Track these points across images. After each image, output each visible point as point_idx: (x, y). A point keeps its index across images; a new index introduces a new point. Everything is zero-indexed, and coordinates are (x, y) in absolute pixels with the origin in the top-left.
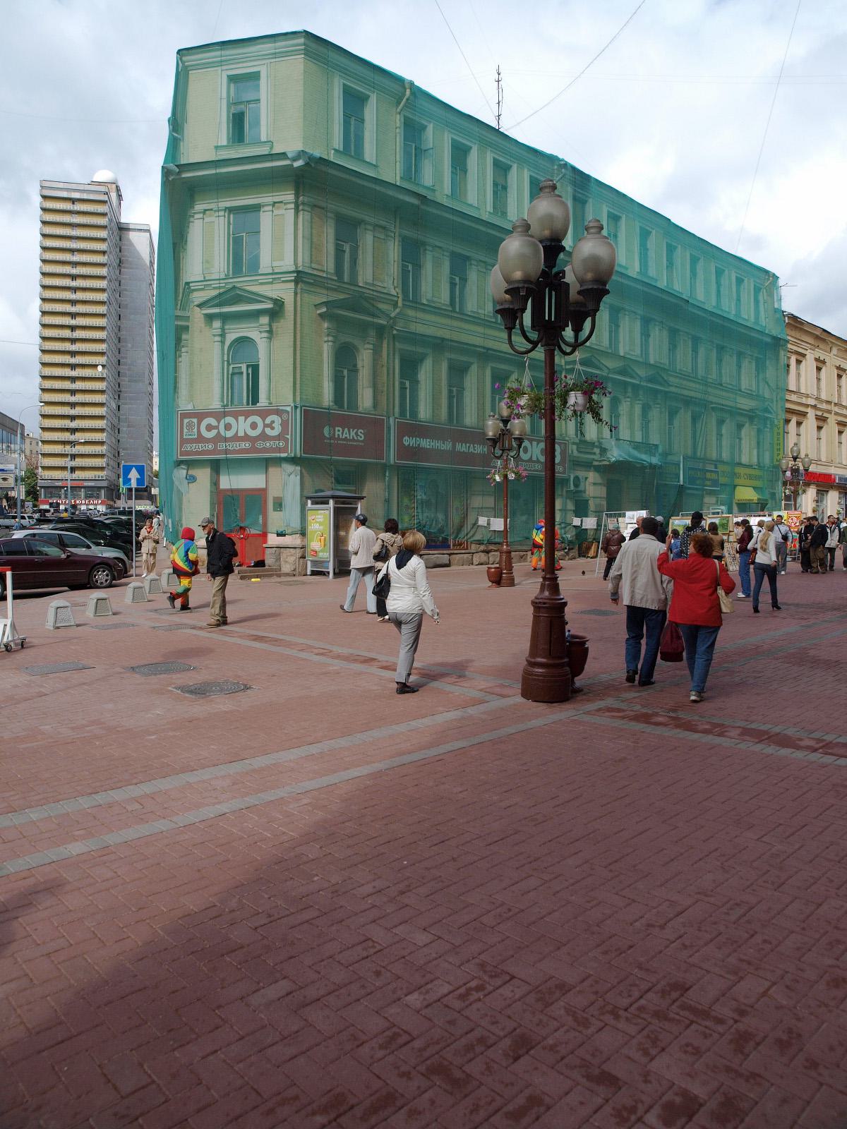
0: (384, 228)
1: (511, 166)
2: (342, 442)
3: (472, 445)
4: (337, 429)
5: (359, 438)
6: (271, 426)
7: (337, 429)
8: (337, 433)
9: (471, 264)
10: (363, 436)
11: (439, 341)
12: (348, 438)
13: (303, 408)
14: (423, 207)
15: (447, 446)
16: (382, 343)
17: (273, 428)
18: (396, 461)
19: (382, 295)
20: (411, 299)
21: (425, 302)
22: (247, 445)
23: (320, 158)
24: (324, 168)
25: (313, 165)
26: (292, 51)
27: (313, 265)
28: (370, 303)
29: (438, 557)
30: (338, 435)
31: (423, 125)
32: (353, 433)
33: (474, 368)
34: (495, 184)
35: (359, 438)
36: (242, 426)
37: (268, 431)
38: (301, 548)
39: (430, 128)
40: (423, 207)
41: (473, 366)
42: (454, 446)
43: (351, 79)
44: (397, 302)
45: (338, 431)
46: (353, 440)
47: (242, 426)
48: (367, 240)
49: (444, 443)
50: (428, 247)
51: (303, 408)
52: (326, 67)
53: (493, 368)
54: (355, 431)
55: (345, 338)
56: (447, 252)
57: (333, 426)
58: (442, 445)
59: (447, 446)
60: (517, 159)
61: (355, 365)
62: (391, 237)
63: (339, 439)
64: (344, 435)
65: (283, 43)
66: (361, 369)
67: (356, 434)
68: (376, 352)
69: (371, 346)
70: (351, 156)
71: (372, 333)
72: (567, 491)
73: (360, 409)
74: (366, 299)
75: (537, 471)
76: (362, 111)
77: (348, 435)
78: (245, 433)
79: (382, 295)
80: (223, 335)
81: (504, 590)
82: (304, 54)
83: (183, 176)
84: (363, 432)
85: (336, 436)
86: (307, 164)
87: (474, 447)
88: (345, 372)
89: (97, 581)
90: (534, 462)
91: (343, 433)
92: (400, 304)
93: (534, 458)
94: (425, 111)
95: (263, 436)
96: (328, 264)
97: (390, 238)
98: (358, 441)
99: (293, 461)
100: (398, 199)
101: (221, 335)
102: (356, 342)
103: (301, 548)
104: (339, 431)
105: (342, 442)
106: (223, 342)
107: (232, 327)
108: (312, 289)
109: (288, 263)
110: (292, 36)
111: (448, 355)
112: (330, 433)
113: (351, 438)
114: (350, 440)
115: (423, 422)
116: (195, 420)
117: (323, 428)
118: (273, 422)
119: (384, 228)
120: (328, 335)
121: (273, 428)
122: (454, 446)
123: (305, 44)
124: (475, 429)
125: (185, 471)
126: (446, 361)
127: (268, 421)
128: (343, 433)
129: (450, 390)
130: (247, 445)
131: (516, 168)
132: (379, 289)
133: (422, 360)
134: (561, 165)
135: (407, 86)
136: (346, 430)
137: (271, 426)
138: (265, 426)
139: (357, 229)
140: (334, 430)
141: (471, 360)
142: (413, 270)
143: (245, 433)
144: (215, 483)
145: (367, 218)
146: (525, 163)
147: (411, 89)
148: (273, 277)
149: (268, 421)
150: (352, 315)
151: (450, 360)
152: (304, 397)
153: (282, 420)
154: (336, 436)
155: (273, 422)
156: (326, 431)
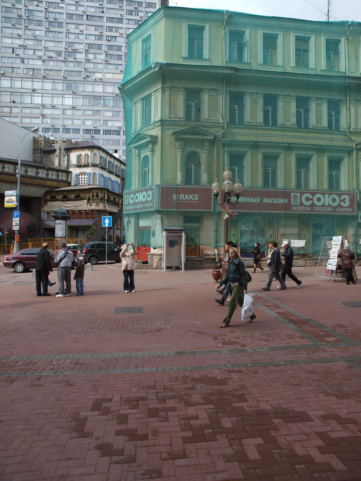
0: (216, 90)
1: (340, 40)
2: (184, 202)
3: (275, 199)
4: (181, 195)
5: (195, 199)
6: (343, 201)
7: (181, 195)
8: (181, 197)
9: (279, 98)
10: (197, 198)
11: (253, 144)
12: (188, 199)
13: (160, 186)
14: (236, 74)
15: (257, 200)
16: (214, 149)
17: (345, 202)
18: (220, 210)
19: (213, 124)
20: (237, 123)
21: (342, 130)
22: (141, 206)
23: (167, 64)
24: (170, 68)
25: (164, 68)
26: (161, 17)
27: (171, 116)
28: (201, 129)
29: (250, 262)
30: (182, 198)
31: (243, 31)
32: (191, 197)
33: (282, 157)
34: (297, 50)
35: (195, 199)
36: (327, 200)
37: (342, 203)
38: (160, 255)
39: (247, 32)
40: (236, 74)
41: (281, 154)
42: (262, 200)
43: (194, 21)
44: (224, 126)
45: (182, 196)
46: (191, 200)
47: (327, 200)
48: (205, 97)
49: (254, 199)
50: (247, 94)
51: (160, 186)
52: (174, 19)
53: (296, 154)
54: (193, 195)
55: (190, 149)
56: (261, 94)
57: (178, 194)
58: (253, 200)
59: (257, 200)
60: (314, 32)
61: (199, 162)
62: (221, 93)
63: (182, 200)
64: (186, 198)
65: (309, 26)
66: (202, 163)
67: (193, 197)
68: (210, 153)
69: (206, 151)
70: (196, 59)
71: (207, 144)
72: (357, 224)
73: (202, 184)
74: (198, 127)
75: (329, 212)
76: (202, 35)
77: (276, 202)
78: (329, 203)
79: (213, 124)
80: (139, 155)
81: (351, 285)
82: (165, 18)
83: (125, 89)
84: (197, 195)
85: (181, 199)
86: (160, 68)
87: (277, 200)
88: (193, 166)
89: (16, 268)
90: (327, 206)
91: (184, 197)
92: (225, 127)
93: (327, 204)
94: (236, 23)
95: (339, 206)
96: (181, 113)
97: (220, 94)
98: (195, 200)
99: (158, 212)
100: (224, 73)
101: (138, 156)
102: (198, 150)
103: (160, 255)
104: (182, 196)
105: (184, 202)
106: (140, 159)
107: (144, 151)
108: (171, 128)
109: (158, 118)
110: (159, 11)
111: (262, 150)
112: (176, 197)
113: (190, 199)
114: (189, 200)
115: (343, 192)
116: (128, 196)
117: (173, 194)
118: (345, 199)
119: (216, 90)
120: (179, 149)
121: (345, 202)
122: (262, 200)
123: (164, 13)
124: (347, 192)
125: (127, 219)
126: (261, 154)
127: (342, 198)
128: (184, 197)
129: (265, 170)
130: (141, 206)
131: (314, 38)
132: (213, 121)
133: (244, 155)
134: (349, 25)
135: (225, 13)
136: (187, 195)
137: (343, 201)
138: (341, 201)
139: (200, 94)
140: (179, 196)
141: (311, 153)
142: (272, 110)
143: (329, 203)
144: (137, 224)
145: (204, 87)
146: (321, 32)
147: (227, 15)
148: (154, 125)
149: (342, 198)
150: (196, 137)
151: (262, 152)
152: (166, 181)
153: (350, 198)
154: (181, 199)
155: (345, 199)
156: (174, 197)
